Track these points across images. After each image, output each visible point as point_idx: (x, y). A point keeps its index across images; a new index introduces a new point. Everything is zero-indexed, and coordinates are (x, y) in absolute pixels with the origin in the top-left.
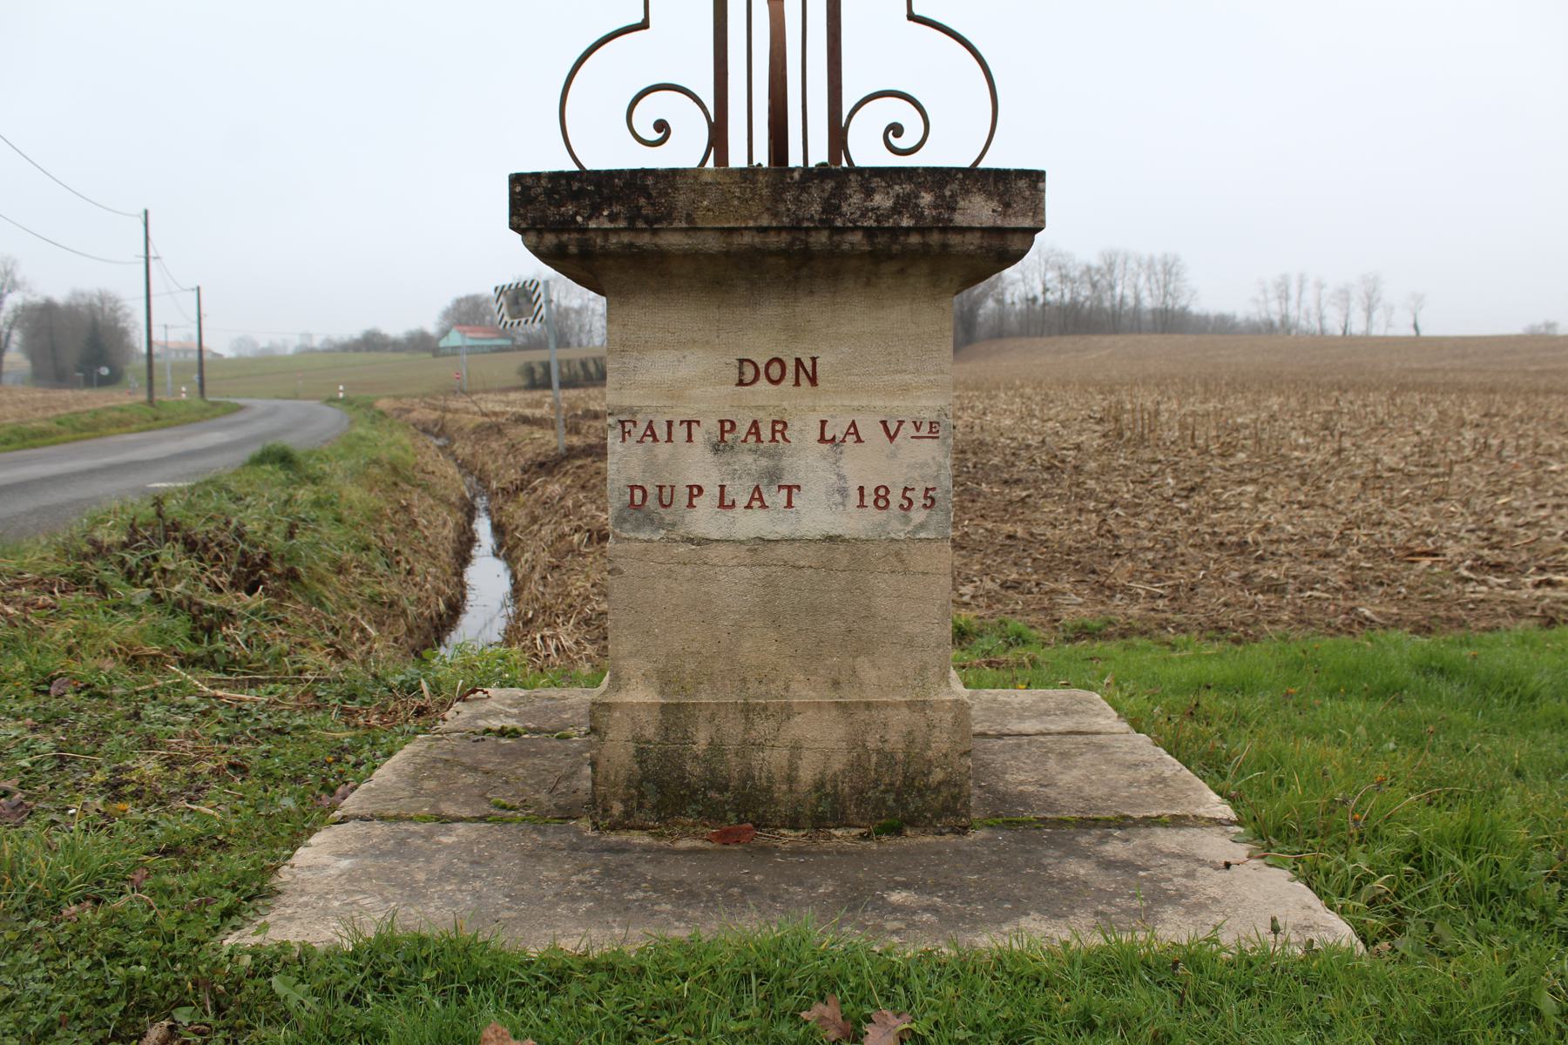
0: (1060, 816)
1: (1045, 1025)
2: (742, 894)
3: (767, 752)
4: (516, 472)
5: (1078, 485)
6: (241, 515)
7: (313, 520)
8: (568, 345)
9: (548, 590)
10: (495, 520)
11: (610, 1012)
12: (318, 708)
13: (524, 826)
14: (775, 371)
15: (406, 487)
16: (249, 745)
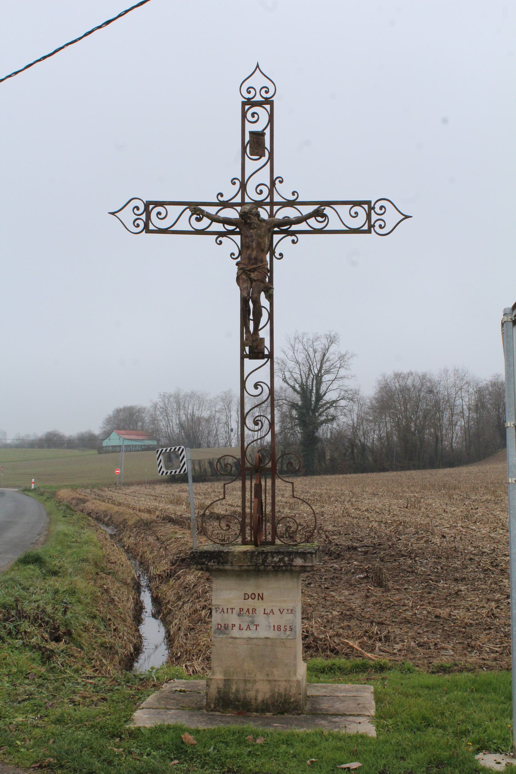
8: (199, 446)
9: (188, 642)
10: (155, 595)
14: (253, 596)
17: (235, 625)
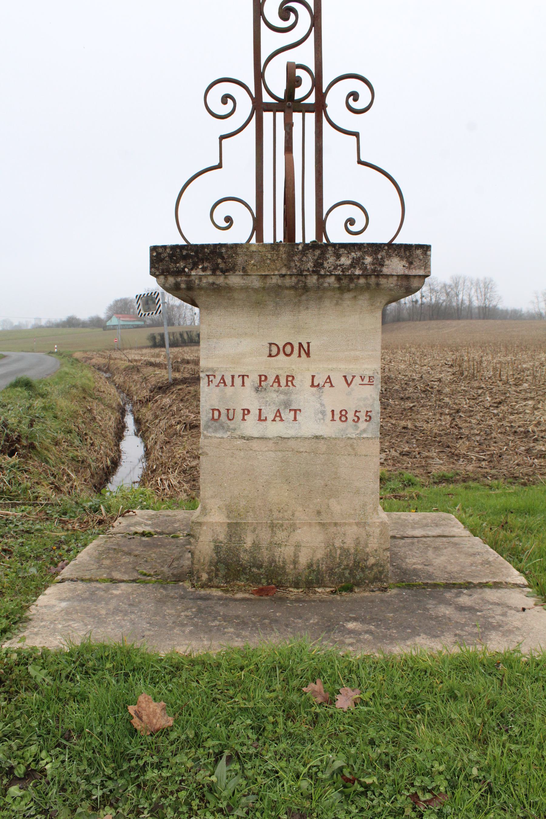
0: (435, 582)
1: (430, 696)
2: (270, 623)
3: (283, 548)
4: (147, 392)
5: (440, 401)
6: (6, 414)
7: (42, 418)
8: (173, 324)
9: (164, 454)
10: (136, 417)
11: (203, 687)
12: (47, 519)
13: (156, 585)
14: (288, 349)
15: (90, 399)
16: (12, 539)
17: (249, 411)
